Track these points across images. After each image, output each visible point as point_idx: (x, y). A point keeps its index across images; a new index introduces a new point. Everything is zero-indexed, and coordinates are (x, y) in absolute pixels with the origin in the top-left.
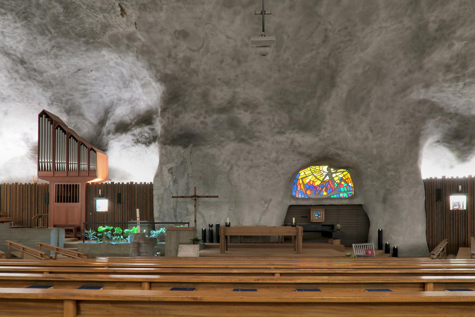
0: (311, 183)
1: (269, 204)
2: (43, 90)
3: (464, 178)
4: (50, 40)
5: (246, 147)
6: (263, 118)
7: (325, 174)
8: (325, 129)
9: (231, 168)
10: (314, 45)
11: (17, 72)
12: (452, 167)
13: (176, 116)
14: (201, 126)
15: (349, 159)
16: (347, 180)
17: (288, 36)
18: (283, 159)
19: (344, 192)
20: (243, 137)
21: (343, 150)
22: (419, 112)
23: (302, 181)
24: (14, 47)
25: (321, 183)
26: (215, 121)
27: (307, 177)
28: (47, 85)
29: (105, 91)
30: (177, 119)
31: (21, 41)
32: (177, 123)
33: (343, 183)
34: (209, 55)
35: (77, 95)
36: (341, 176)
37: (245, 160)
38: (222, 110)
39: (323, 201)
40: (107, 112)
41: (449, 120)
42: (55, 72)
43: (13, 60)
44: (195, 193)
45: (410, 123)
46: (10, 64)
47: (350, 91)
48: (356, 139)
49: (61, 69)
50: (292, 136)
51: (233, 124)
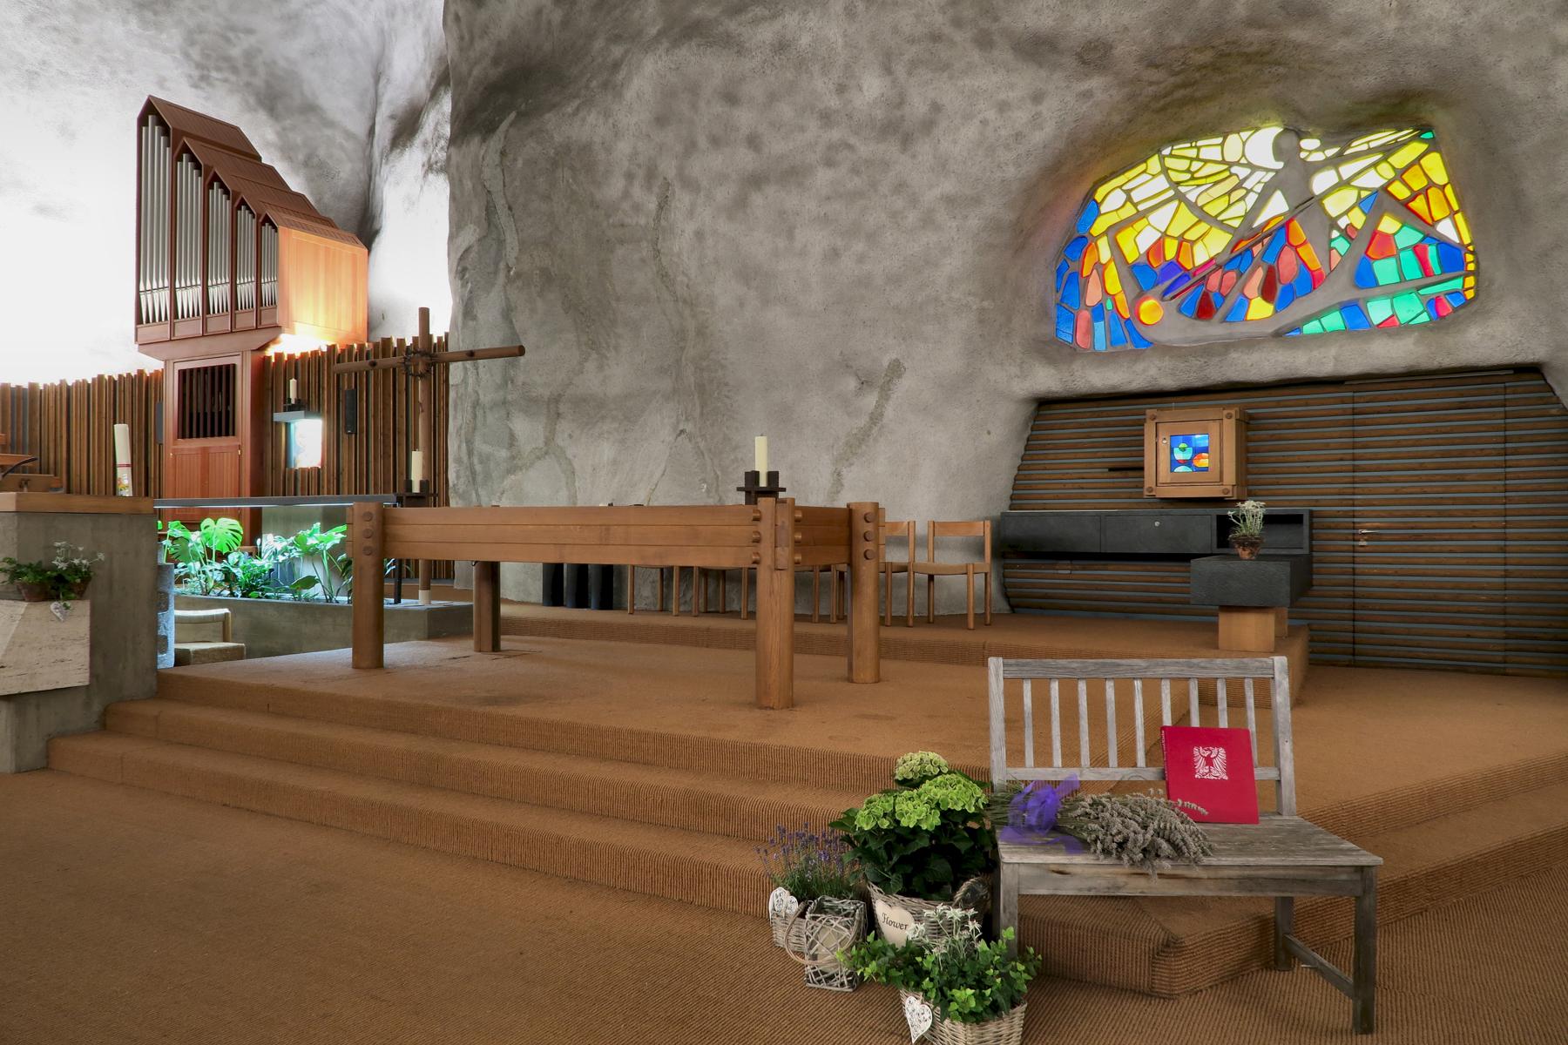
0: (1170, 252)
1: (885, 393)
2: (144, 23)
5: (715, 66)
7: (1256, 182)
9: (663, 205)
15: (1391, 24)
16: (1419, 205)
18: (936, 108)
19: (1403, 285)
23: (1115, 246)
27: (1141, 215)
30: (482, 15)
33: (1388, 225)
36: (1373, 180)
37: (715, 142)
39: (1234, 355)
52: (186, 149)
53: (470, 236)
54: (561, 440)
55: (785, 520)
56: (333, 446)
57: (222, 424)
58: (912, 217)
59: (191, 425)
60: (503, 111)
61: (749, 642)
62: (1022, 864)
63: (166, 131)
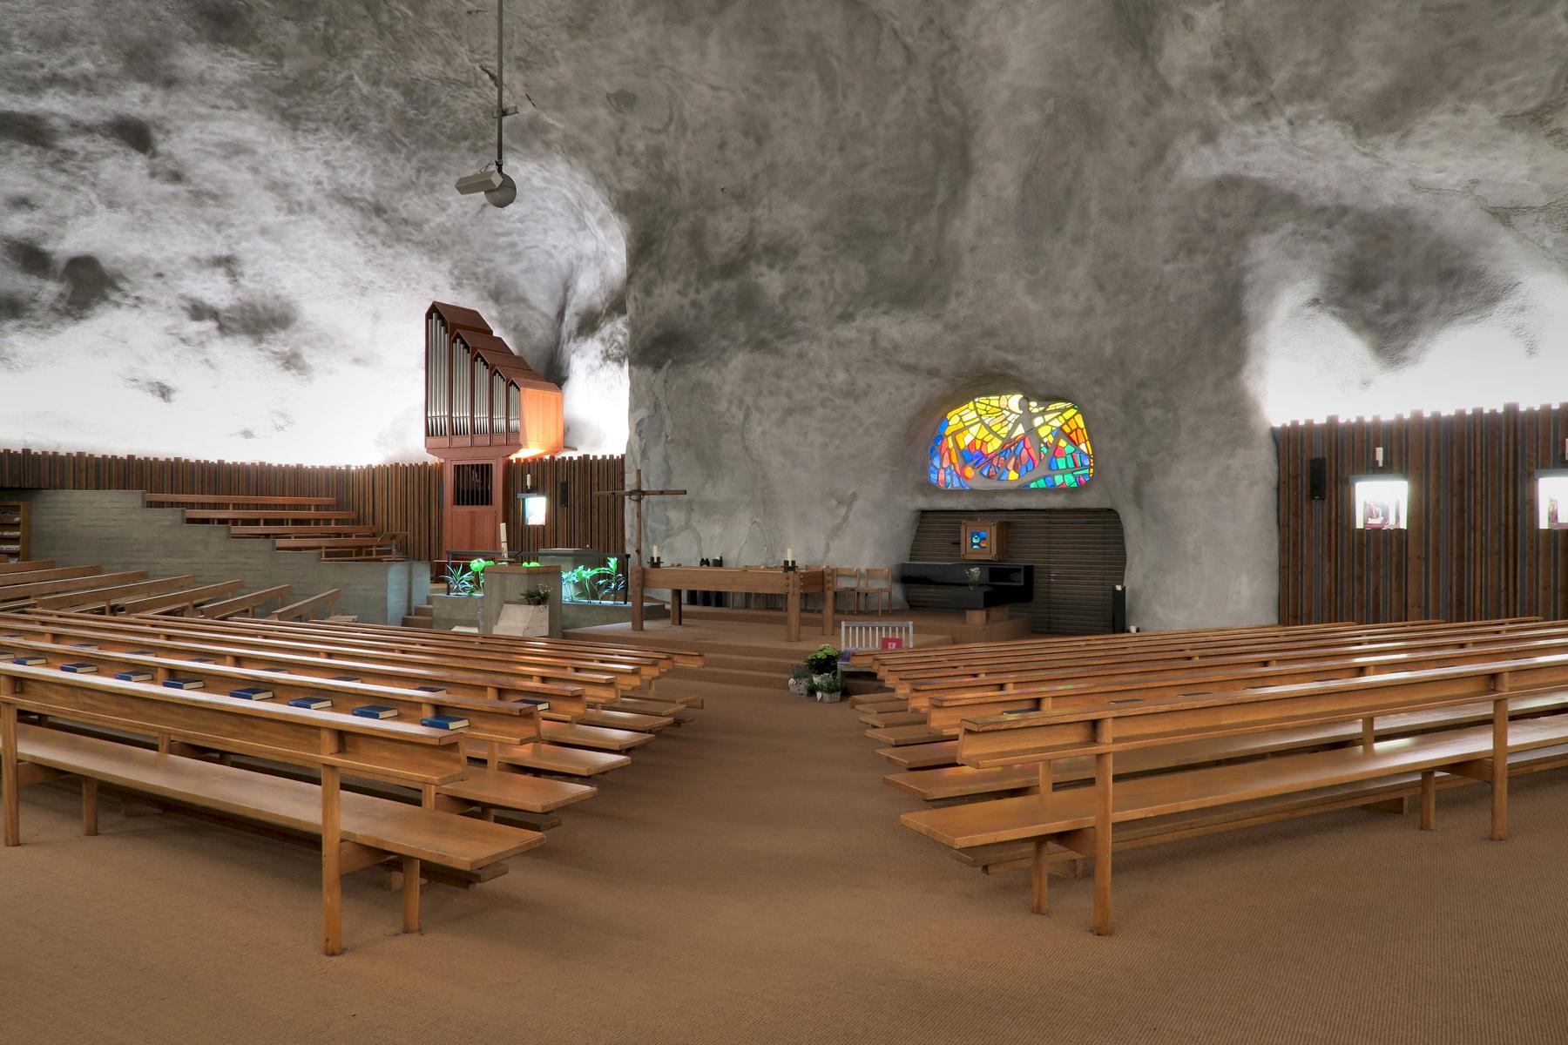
1: (849, 507)
2: (431, 259)
3: (1400, 420)
4: (408, 159)
5: (771, 362)
6: (811, 280)
7: (1012, 418)
8: (958, 295)
10: (894, 71)
11: (373, 231)
12: (1366, 383)
16: (1073, 436)
17: (839, 59)
18: (869, 386)
20: (764, 334)
21: (1019, 350)
22: (1226, 215)
23: (955, 441)
24: (358, 185)
25: (1003, 446)
26: (715, 300)
28: (435, 248)
29: (551, 240)
30: (650, 301)
31: (363, 171)
33: (1063, 443)
34: (689, 135)
35: (501, 259)
36: (1057, 423)
37: (771, 393)
38: (730, 269)
40: (567, 287)
41: (1325, 232)
42: (441, 219)
43: (362, 210)
44: (639, 482)
45: (1205, 251)
46: (357, 220)
47: (1028, 177)
48: (1057, 314)
49: (450, 211)
50: (871, 322)
51: (748, 302)
52: (458, 336)
53: (643, 413)
54: (694, 523)
55: (797, 578)
56: (552, 513)
57: (484, 498)
58: (860, 430)
59: (461, 498)
60: (666, 356)
61: (784, 621)
62: (842, 666)
63: (444, 324)
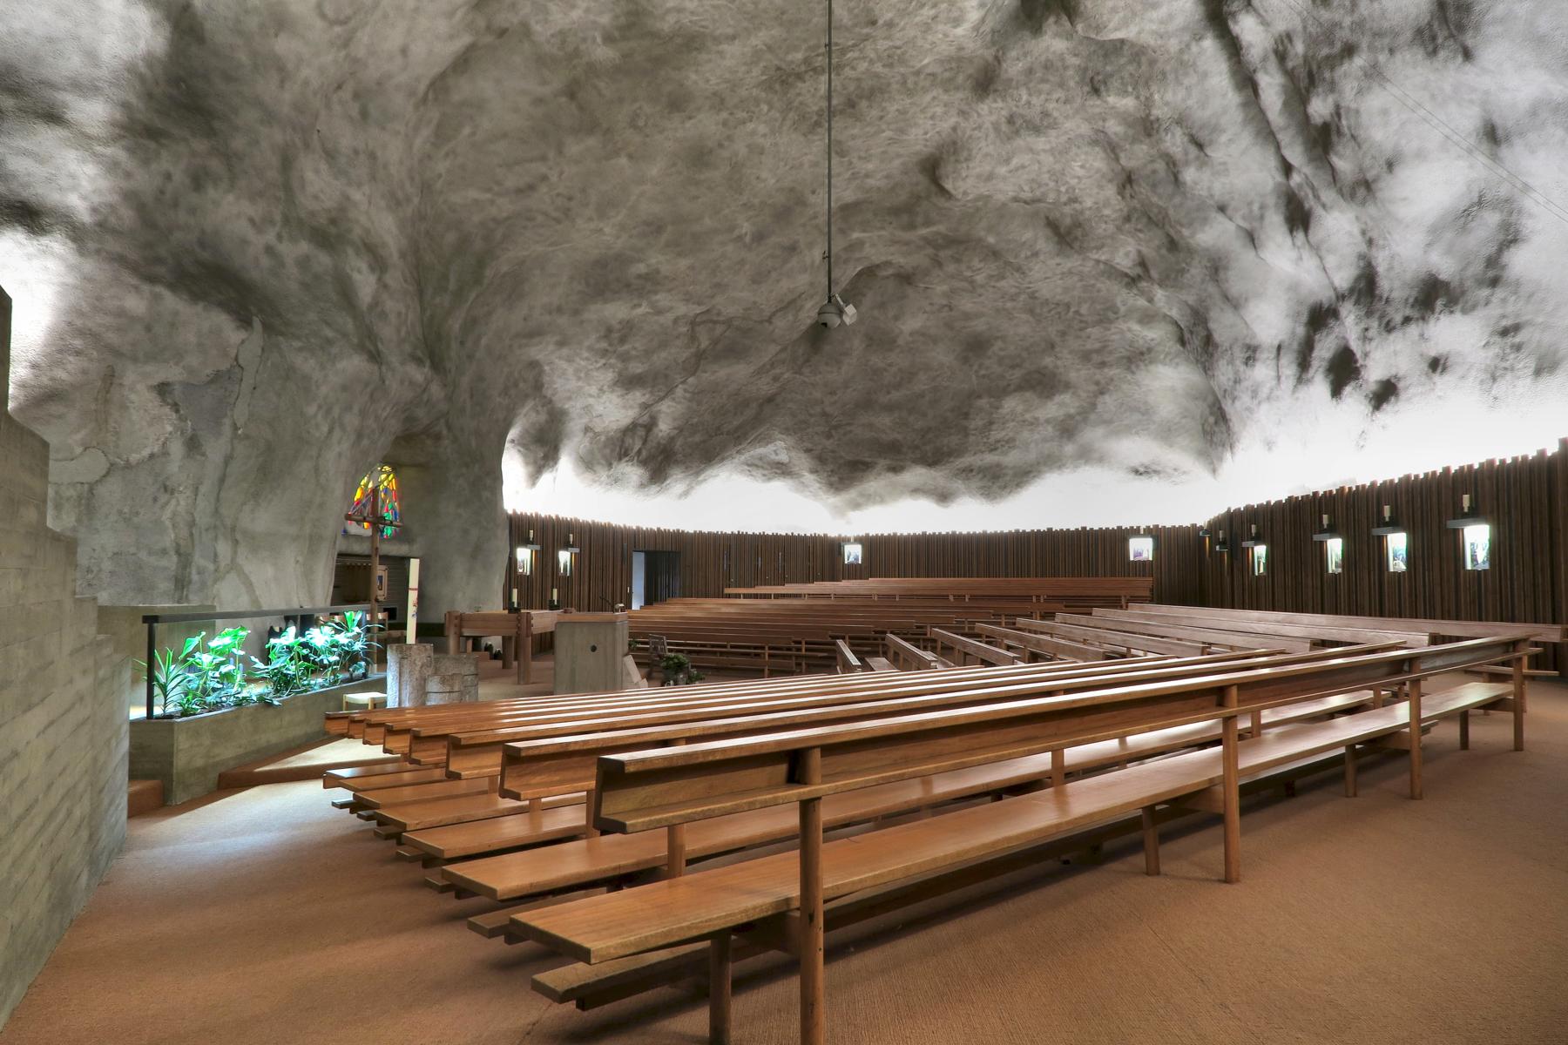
13: (199, 180)
14: (265, 262)
17: (473, 134)
32: (192, 211)
34: (343, 53)
54: (240, 560)
